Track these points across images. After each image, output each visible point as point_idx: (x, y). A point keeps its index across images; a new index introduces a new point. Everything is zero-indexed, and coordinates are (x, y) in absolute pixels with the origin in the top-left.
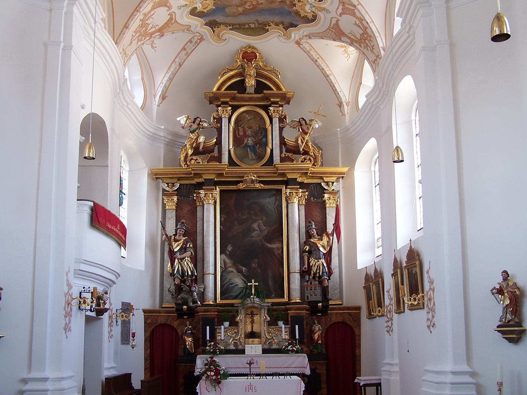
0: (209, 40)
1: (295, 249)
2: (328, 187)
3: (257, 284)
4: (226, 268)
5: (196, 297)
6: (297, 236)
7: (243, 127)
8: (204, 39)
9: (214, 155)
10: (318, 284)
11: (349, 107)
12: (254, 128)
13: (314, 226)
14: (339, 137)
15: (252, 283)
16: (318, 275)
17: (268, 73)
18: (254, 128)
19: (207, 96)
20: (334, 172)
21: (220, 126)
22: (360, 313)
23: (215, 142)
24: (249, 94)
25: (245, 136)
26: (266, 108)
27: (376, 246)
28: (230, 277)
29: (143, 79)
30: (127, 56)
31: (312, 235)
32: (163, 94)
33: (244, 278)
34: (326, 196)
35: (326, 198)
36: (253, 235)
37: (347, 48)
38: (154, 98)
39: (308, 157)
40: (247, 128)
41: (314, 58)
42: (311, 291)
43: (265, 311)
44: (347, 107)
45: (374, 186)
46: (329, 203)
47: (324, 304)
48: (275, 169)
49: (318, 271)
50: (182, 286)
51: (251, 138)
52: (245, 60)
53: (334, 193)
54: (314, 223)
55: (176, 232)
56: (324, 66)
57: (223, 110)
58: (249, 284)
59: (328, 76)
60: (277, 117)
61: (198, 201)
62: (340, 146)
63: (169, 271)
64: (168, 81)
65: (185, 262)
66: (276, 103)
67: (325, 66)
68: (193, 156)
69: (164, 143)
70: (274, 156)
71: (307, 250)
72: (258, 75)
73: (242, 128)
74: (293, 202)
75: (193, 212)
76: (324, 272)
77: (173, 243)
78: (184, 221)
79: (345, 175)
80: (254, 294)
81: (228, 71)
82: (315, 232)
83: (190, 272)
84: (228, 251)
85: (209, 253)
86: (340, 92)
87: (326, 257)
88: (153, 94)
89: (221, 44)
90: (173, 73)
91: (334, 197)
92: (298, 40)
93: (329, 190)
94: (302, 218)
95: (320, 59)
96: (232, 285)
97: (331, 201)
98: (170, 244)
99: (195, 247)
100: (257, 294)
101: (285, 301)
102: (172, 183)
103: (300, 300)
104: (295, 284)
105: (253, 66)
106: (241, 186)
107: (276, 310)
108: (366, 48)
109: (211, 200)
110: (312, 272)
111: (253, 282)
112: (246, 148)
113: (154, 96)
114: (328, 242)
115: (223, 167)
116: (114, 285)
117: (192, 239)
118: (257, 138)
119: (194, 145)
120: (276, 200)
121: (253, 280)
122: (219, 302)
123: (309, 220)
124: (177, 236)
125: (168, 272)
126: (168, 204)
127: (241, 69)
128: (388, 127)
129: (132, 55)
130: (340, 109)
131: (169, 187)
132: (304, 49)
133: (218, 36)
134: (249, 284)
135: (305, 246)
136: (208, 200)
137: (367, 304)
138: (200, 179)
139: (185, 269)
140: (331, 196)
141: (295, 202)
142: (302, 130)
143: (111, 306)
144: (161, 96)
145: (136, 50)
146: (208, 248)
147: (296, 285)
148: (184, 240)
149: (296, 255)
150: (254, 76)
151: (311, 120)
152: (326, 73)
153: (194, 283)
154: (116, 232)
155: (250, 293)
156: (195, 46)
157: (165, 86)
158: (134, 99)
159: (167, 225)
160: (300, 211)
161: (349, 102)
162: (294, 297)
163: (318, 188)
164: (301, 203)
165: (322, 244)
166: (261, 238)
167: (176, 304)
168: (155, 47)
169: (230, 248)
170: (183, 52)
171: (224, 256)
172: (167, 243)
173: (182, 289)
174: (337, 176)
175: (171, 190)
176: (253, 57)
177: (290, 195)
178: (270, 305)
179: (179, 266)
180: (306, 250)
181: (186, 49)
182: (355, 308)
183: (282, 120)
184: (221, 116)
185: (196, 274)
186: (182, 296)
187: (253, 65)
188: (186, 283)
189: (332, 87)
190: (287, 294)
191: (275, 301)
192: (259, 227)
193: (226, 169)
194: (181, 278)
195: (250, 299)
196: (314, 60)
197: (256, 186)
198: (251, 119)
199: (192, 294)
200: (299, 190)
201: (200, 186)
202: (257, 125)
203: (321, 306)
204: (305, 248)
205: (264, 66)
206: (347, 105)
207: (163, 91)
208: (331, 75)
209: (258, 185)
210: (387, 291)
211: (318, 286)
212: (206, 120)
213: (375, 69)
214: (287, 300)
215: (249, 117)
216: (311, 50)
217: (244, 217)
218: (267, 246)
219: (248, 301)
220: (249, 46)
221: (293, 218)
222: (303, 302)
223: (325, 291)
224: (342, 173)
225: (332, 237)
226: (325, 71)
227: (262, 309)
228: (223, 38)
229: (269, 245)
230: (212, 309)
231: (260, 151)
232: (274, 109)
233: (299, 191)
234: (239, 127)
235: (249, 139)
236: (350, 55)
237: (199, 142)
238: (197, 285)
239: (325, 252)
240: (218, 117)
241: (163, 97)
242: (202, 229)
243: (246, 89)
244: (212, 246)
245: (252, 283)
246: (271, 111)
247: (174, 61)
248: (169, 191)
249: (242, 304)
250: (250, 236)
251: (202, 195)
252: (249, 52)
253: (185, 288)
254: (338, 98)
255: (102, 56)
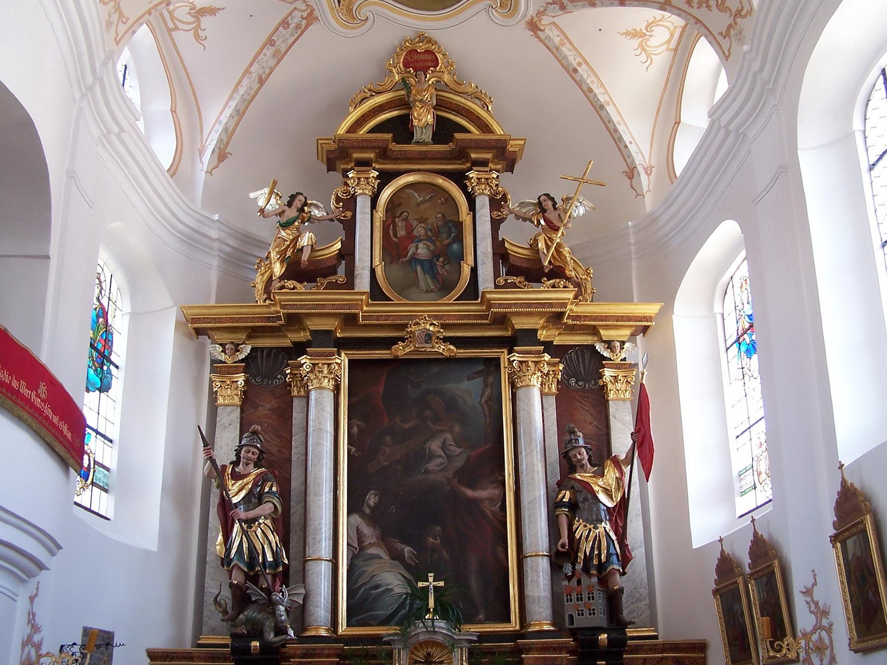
0: (326, 17)
1: (536, 498)
2: (611, 354)
3: (442, 584)
4: (362, 548)
5: (283, 618)
6: (539, 467)
7: (406, 220)
8: (316, 18)
9: (337, 281)
10: (596, 585)
11: (651, 177)
12: (432, 220)
13: (581, 442)
14: (632, 241)
15: (428, 582)
16: (595, 562)
17: (463, 100)
18: (432, 220)
19: (322, 148)
20: (626, 316)
21: (352, 217)
22: (705, 658)
23: (339, 250)
24: (418, 143)
25: (411, 237)
26: (459, 178)
27: (737, 490)
28: (373, 571)
29: (175, 112)
30: (124, 20)
31: (579, 464)
32: (220, 148)
33: (408, 574)
34: (608, 373)
35: (607, 378)
36: (428, 468)
37: (646, 37)
38: (200, 156)
39: (562, 282)
40: (416, 221)
41: (569, 64)
42: (580, 602)
43: (462, 654)
44: (647, 176)
45: (722, 348)
46: (614, 390)
47: (614, 635)
48: (485, 308)
49: (596, 552)
50: (248, 588)
51: (425, 242)
52: (411, 69)
53: (623, 366)
54: (581, 434)
55: (238, 455)
56: (593, 82)
57: (359, 179)
58: (420, 584)
59: (602, 107)
60: (486, 195)
61: (294, 386)
62: (634, 264)
63: (218, 552)
64: (231, 116)
65: (259, 529)
66: (484, 163)
67: (596, 83)
68: (286, 281)
69: (219, 255)
70: (480, 279)
71: (567, 500)
72: (441, 104)
73: (403, 220)
74: (528, 386)
75: (284, 414)
76: (611, 554)
77: (230, 483)
78: (258, 428)
79: (654, 323)
80: (433, 609)
81: (372, 96)
82: (587, 457)
83: (271, 556)
84: (369, 506)
85: (320, 507)
86: (631, 143)
87: (614, 518)
88: (198, 149)
89: (356, 31)
90: (246, 99)
91: (626, 376)
92: (534, 16)
93: (613, 361)
94: (551, 426)
95: (584, 66)
96: (377, 591)
97: (619, 386)
98: (223, 487)
99: (285, 495)
100: (442, 610)
101: (511, 629)
102: (232, 343)
103: (553, 625)
104: (538, 586)
105: (430, 82)
106: (401, 350)
107: (490, 652)
108: (704, 5)
109: (326, 380)
110: (579, 554)
111: (430, 578)
112: (413, 264)
113: (200, 151)
114: (619, 480)
115: (356, 300)
116: (43, 571)
117: (277, 473)
118: (437, 243)
119: (289, 254)
120: (486, 385)
121: (430, 575)
122: (344, 633)
123: (571, 425)
124: (239, 465)
125: (217, 555)
126: (224, 392)
127: (403, 89)
128: (779, 168)
129: (138, 22)
130: (631, 182)
131: (227, 351)
132: (546, 41)
133: (349, 10)
134: (420, 584)
135: (560, 491)
136: (321, 380)
137: (726, 637)
138: (302, 334)
139: (259, 547)
140: (621, 374)
141: (534, 385)
142: (545, 222)
143: (35, 632)
144: (217, 150)
145: (149, 12)
146: (318, 494)
147: (542, 588)
148: (258, 475)
149: (538, 513)
150: (430, 103)
151: (567, 200)
152: (599, 100)
153: (278, 583)
154: (32, 405)
155: (422, 607)
156: (296, 36)
157: (226, 129)
158: (138, 120)
159: (218, 442)
160: (544, 409)
161: (651, 167)
162: (537, 617)
163: (587, 356)
164: (546, 390)
165: (605, 486)
166: (449, 474)
167: (234, 636)
168: (204, 38)
169: (372, 499)
170: (268, 48)
171: (356, 518)
172: (215, 484)
173: (249, 597)
174: (632, 326)
175: (229, 361)
176: (429, 64)
177: (520, 367)
178: (475, 638)
179: (242, 538)
180: (564, 500)
181: (275, 42)
182: (693, 648)
183: (497, 203)
184: (354, 193)
185: (286, 561)
186: (249, 616)
187: (428, 81)
188: (260, 585)
189: (612, 131)
190: (517, 611)
191: (486, 630)
192: (444, 447)
193: (365, 308)
194: (246, 570)
195: (422, 621)
196: (571, 70)
197: (436, 350)
198: (424, 202)
199: (274, 611)
200: (544, 356)
201: (300, 349)
202: (440, 215)
203: (606, 640)
204: (560, 496)
205: (454, 82)
206: (646, 173)
207: (220, 140)
208: (608, 104)
209: (443, 347)
210: (804, 590)
211: (598, 590)
212: (319, 204)
213: (729, 50)
214: (518, 628)
215: (420, 197)
216: (563, 44)
217: (407, 426)
218: (465, 494)
219: (419, 629)
220: (419, 37)
221: (530, 422)
222: (559, 631)
223: (613, 599)
224: (644, 317)
225: (630, 466)
226: (595, 95)
227: (454, 648)
228: (359, 14)
229: (470, 493)
230: (324, 649)
231: (446, 270)
232: (480, 177)
233: (543, 359)
234: (396, 219)
235: (421, 245)
236: (652, 56)
237: (300, 247)
238: (286, 587)
239: (610, 505)
240: (347, 196)
241: (221, 155)
242: (304, 452)
243: (412, 135)
244: (328, 491)
245: (428, 582)
246: (473, 181)
247: (247, 71)
248: (225, 363)
249: (404, 636)
250: (423, 471)
251: (306, 368)
252: (419, 51)
253: (255, 593)
254: (626, 158)
255: (66, 18)
